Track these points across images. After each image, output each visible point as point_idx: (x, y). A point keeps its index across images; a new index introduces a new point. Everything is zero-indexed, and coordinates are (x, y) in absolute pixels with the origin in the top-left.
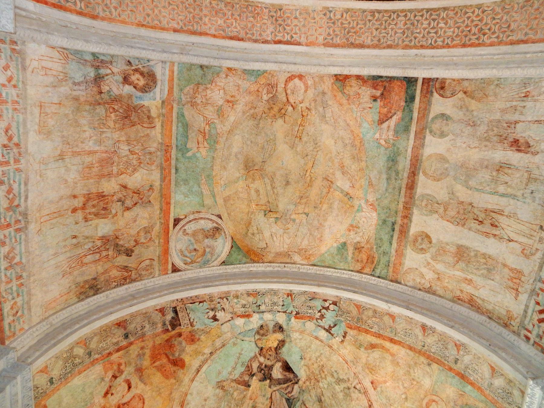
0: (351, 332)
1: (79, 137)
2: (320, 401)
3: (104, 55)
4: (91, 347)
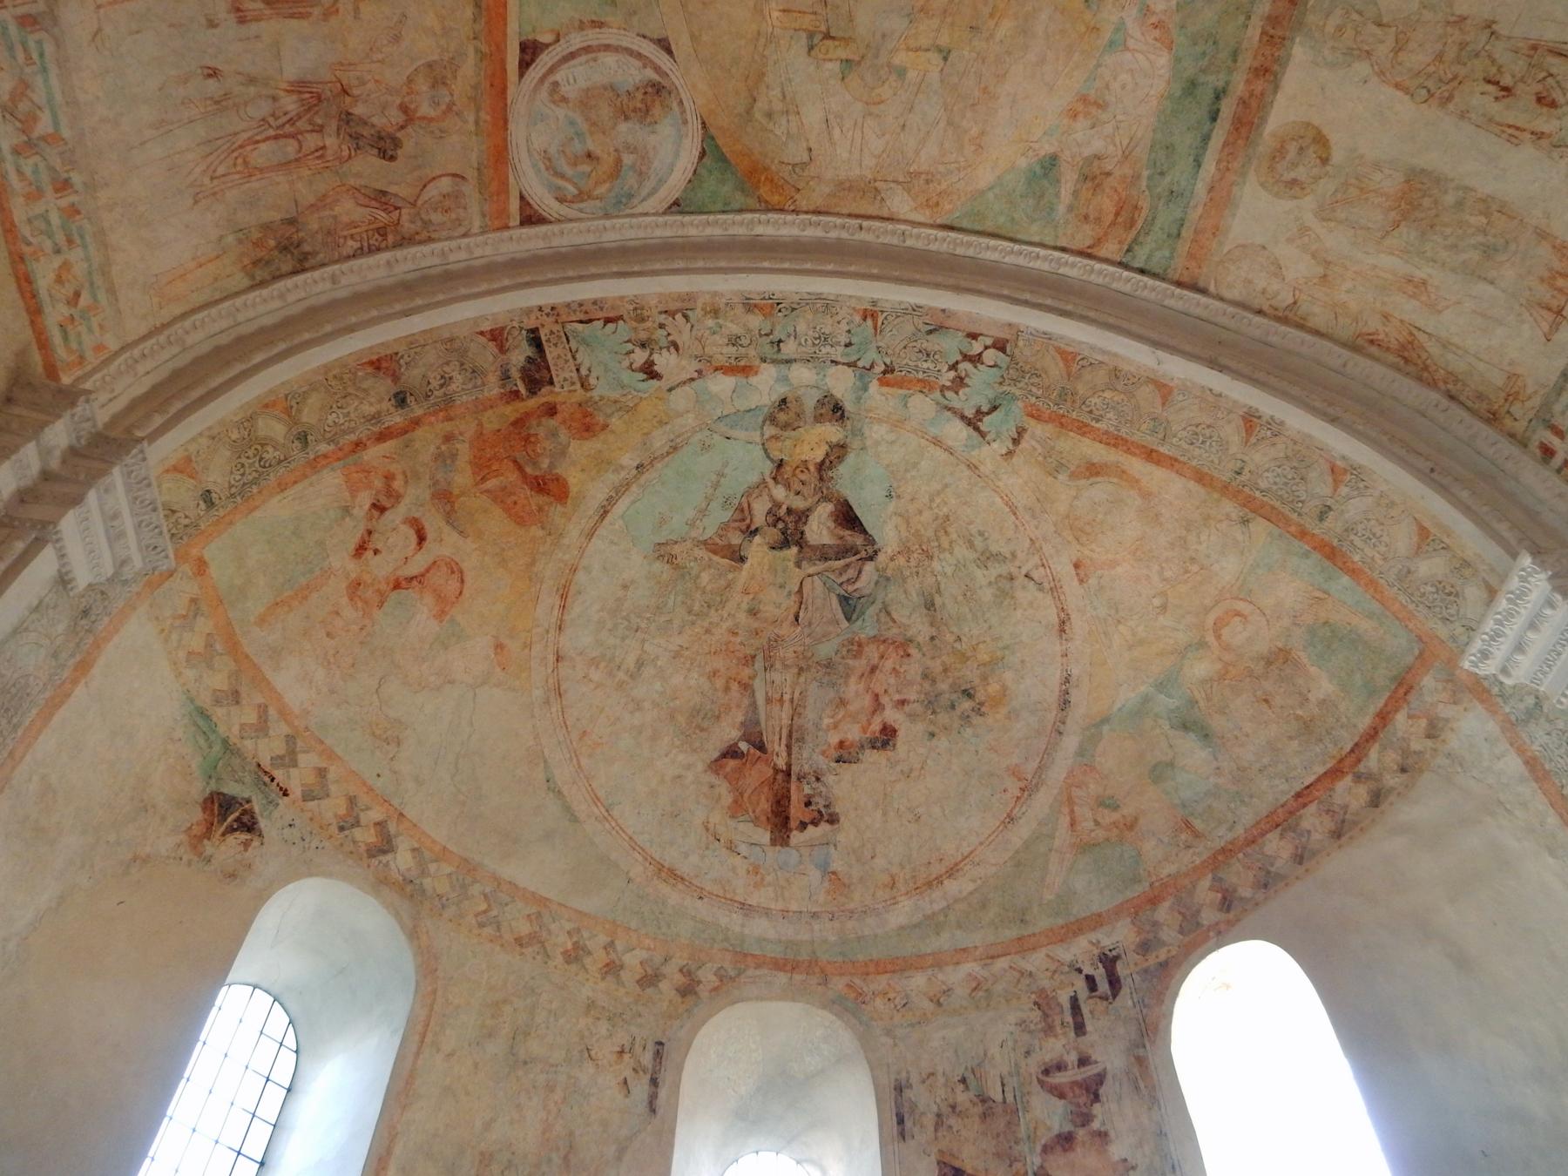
0: (1037, 430)
2: (930, 605)
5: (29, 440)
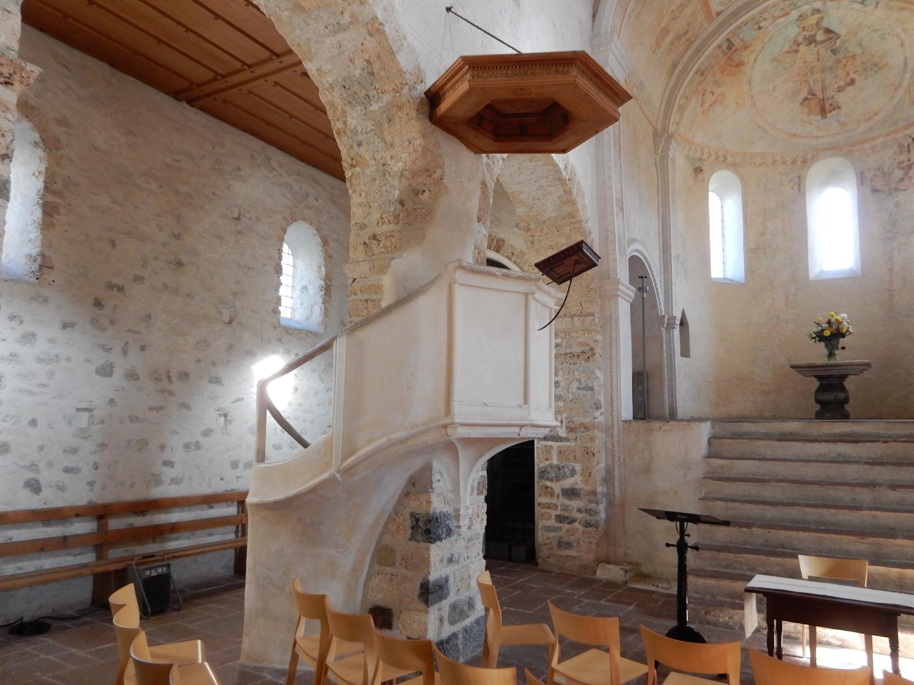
2: (860, 45)
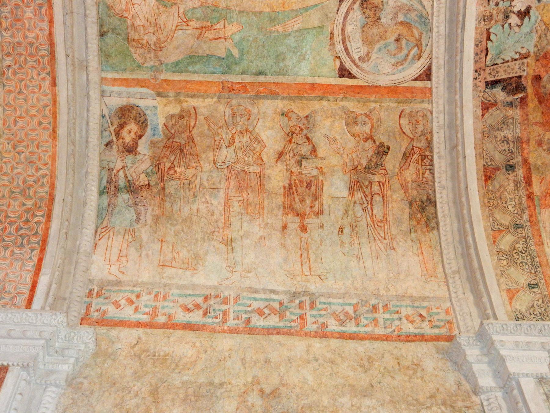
1: (206, 219)
3: (101, 180)
4: (507, 224)
5: (471, 368)
